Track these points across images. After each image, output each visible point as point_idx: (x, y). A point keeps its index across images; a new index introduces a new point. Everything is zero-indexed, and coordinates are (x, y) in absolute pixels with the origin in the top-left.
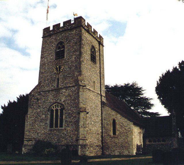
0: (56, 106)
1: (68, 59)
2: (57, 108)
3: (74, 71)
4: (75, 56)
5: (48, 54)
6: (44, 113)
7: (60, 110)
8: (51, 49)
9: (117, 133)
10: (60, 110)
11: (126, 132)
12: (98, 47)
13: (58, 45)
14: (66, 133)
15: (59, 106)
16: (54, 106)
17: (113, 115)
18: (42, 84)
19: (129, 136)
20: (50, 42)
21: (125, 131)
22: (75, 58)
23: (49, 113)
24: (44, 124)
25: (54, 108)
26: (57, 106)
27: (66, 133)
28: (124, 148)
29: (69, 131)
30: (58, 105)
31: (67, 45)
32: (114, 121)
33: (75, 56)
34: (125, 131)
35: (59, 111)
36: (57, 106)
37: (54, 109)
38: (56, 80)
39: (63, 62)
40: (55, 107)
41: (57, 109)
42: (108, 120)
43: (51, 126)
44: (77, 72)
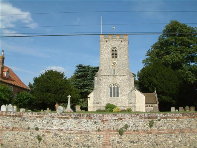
20: (107, 46)
23: (109, 88)
25: (112, 86)
34: (141, 100)
37: (113, 87)
38: (113, 71)
43: (111, 96)
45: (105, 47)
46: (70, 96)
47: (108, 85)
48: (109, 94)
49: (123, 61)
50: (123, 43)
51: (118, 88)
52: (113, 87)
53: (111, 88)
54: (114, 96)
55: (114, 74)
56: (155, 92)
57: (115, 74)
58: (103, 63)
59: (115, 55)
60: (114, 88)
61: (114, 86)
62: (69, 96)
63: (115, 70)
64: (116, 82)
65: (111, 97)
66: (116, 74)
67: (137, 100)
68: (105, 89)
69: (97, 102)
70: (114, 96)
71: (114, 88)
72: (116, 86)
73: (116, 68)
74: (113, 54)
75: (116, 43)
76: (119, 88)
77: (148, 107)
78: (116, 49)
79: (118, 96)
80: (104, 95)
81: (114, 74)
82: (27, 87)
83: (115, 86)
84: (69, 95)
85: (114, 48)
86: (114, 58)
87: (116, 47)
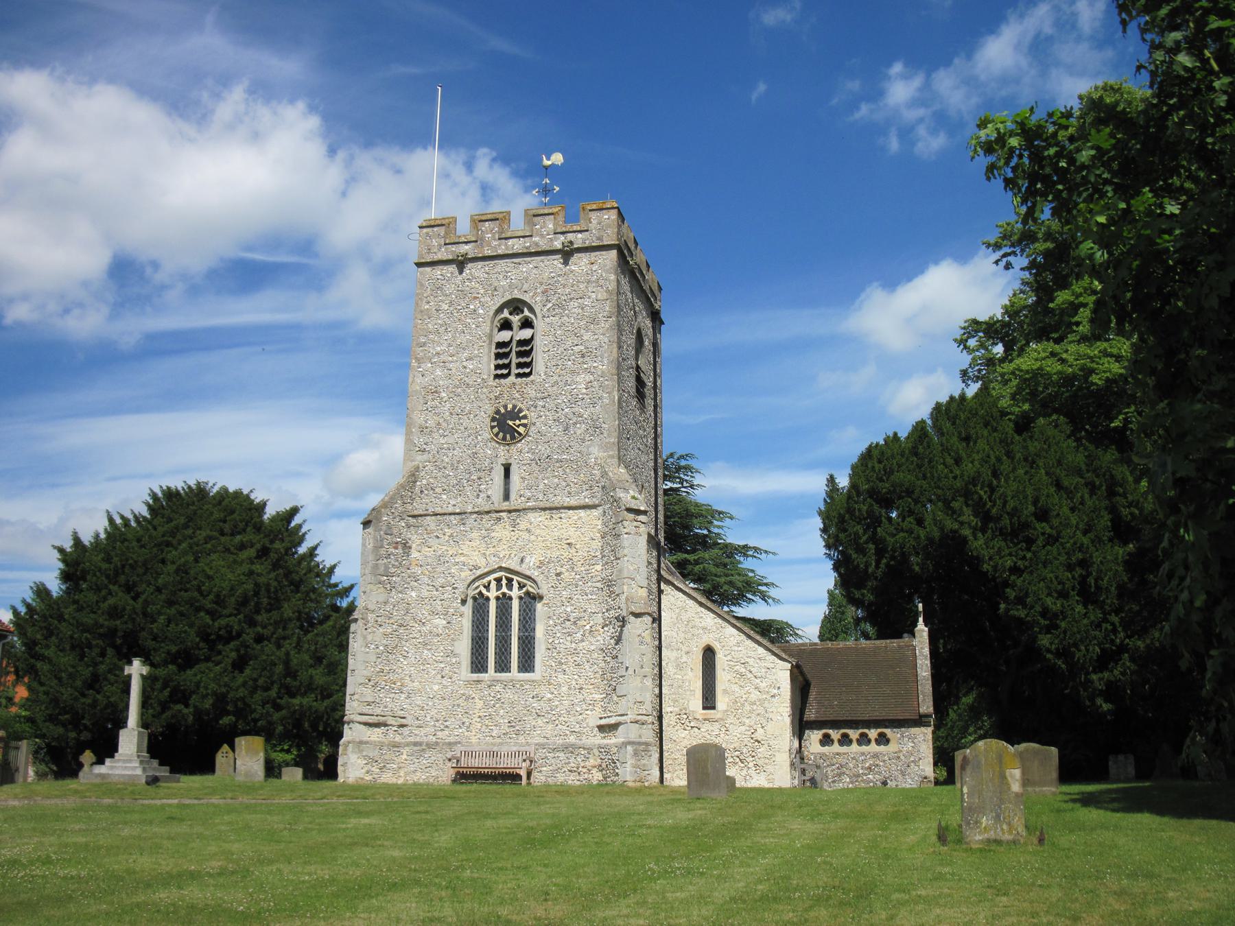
0: (499, 580)
1: (557, 383)
2: (504, 589)
3: (583, 441)
4: (589, 377)
5: (450, 345)
6: (439, 608)
7: (498, 598)
8: (467, 326)
9: (722, 702)
10: (498, 598)
11: (762, 702)
12: (650, 332)
13: (500, 310)
14: (549, 696)
15: (515, 584)
16: (489, 583)
17: (704, 628)
18: (424, 482)
19: (771, 716)
20: (462, 293)
21: (755, 695)
22: (589, 386)
23: (468, 610)
24: (439, 656)
25: (487, 587)
26: (504, 582)
27: (549, 696)
28: (751, 765)
29: (564, 689)
30: (510, 581)
31: (547, 320)
32: (709, 654)
33: (589, 377)
34: (755, 695)
35: (515, 604)
36: (504, 582)
37: (493, 594)
38: (499, 473)
39: (533, 394)
40: (493, 584)
41: (504, 594)
42: (685, 649)
43: (478, 664)
44: (601, 447)
45: (451, 304)
46: (144, 663)
47: (461, 587)
48: (464, 647)
49: (574, 401)
50: (580, 263)
51: (531, 599)
52: (493, 594)
53: (480, 603)
54: (503, 666)
55: (507, 497)
56: (921, 627)
57: (513, 496)
58: (431, 423)
59: (520, 354)
60: (504, 601)
61: (499, 587)
62: (136, 669)
63: (513, 469)
64: (513, 565)
65: (475, 676)
66: (515, 501)
67: (725, 692)
68: (434, 613)
69: (366, 710)
70: (503, 666)
71: (504, 601)
72: (515, 593)
73: (519, 454)
74: (519, 365)
75: (528, 267)
76: (539, 606)
77: (855, 747)
78: (526, 313)
79: (527, 664)
80: (425, 662)
81: (507, 497)
82: (816, 644)
83: (510, 586)
84: (136, 663)
85: (516, 305)
86: (512, 378)
87: (526, 298)
